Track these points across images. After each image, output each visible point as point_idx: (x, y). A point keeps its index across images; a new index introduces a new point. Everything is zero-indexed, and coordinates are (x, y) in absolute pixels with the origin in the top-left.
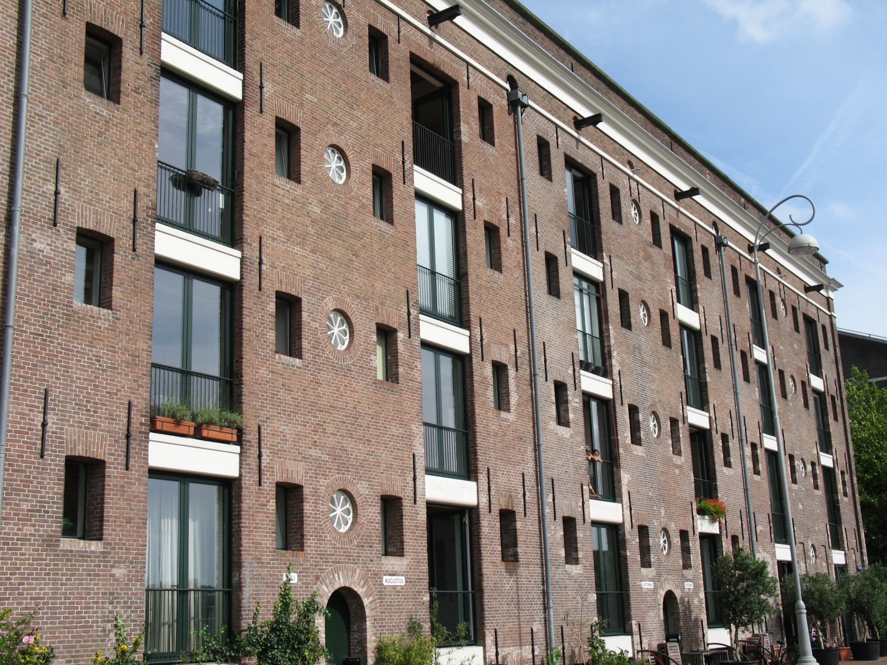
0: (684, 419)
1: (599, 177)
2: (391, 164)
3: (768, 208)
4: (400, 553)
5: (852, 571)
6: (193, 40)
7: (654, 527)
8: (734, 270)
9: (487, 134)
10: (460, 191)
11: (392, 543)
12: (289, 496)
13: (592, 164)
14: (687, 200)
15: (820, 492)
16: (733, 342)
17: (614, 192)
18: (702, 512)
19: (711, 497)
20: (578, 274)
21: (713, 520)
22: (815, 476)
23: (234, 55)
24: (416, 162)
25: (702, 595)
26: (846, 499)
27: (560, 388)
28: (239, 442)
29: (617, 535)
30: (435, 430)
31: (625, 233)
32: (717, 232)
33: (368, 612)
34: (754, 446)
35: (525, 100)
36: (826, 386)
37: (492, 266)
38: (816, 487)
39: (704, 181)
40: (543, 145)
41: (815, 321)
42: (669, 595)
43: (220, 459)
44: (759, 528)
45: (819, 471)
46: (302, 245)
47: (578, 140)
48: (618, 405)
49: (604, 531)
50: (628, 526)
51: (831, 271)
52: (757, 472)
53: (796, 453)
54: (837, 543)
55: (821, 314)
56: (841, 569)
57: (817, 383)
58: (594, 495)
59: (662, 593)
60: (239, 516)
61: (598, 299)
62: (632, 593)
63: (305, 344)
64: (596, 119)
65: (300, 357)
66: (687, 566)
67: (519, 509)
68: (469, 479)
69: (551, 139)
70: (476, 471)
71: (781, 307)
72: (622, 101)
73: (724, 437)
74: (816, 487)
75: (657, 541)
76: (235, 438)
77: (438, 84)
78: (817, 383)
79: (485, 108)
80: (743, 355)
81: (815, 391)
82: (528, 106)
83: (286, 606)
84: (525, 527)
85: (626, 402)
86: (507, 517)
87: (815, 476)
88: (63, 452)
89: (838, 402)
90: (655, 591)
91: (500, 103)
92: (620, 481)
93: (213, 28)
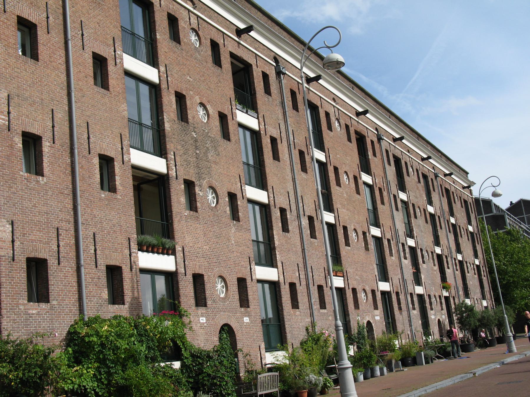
0: (435, 251)
1: (254, 67)
2: (106, 52)
3: (307, 41)
4: (325, 308)
5: (489, 308)
6: (134, 55)
7: (359, 289)
8: (387, 151)
9: (268, 91)
10: (324, 154)
11: (244, 302)
12: (198, 280)
13: (317, 102)
14: (362, 116)
15: (476, 276)
16: (292, 143)
17: (406, 163)
18: (444, 288)
19: (169, 238)
20: (241, 125)
21: (447, 291)
22: (474, 269)
23: (153, 60)
24: (362, 171)
25: (447, 320)
26: (485, 278)
27: (106, 162)
28: (343, 277)
29: (422, 299)
30: (256, 243)
31: (335, 137)
32: (378, 132)
33: (374, 329)
34: (403, 245)
35: (283, 71)
36: (474, 230)
37: (337, 185)
38: (475, 274)
39: (454, 169)
40: (387, 151)
41: (317, 107)
42: (439, 320)
43: (166, 263)
44: (460, 293)
45: (457, 261)
46: (344, 208)
47: (239, 43)
48: (383, 239)
49: (267, 286)
50: (392, 292)
51: (471, 177)
52: (457, 270)
53: (468, 260)
54: (484, 298)
55: (353, 121)
56: (486, 308)
57: (431, 209)
58: (259, 264)
59: (437, 320)
60: (346, 299)
61: (406, 208)
62: (429, 320)
63: (199, 205)
64: (402, 138)
65: (350, 246)
66: (442, 309)
67: (400, 291)
68: (386, 282)
69: (220, 41)
70: (388, 279)
71: (410, 170)
72: (266, 18)
73: (446, 257)
74: (475, 274)
75: (361, 296)
76: (342, 275)
77: (242, 66)
78: (431, 209)
79: (265, 76)
80: (395, 196)
81: (402, 201)
82: (286, 74)
83: (359, 327)
84: (301, 290)
85: (342, 224)
86: (292, 286)
87: (474, 269)
88: (25, 256)
89: (478, 236)
90: (435, 319)
91: (375, 140)
92: (421, 278)
93: (142, 47)
